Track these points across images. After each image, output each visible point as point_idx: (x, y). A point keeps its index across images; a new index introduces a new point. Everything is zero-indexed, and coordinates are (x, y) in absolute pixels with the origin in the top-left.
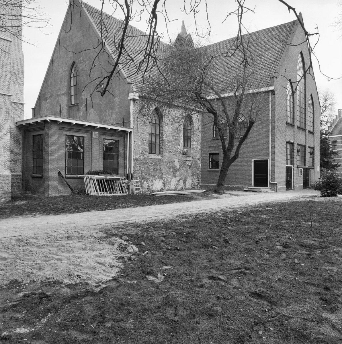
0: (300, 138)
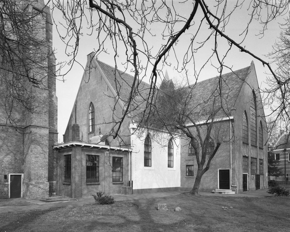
0: (252, 153)
